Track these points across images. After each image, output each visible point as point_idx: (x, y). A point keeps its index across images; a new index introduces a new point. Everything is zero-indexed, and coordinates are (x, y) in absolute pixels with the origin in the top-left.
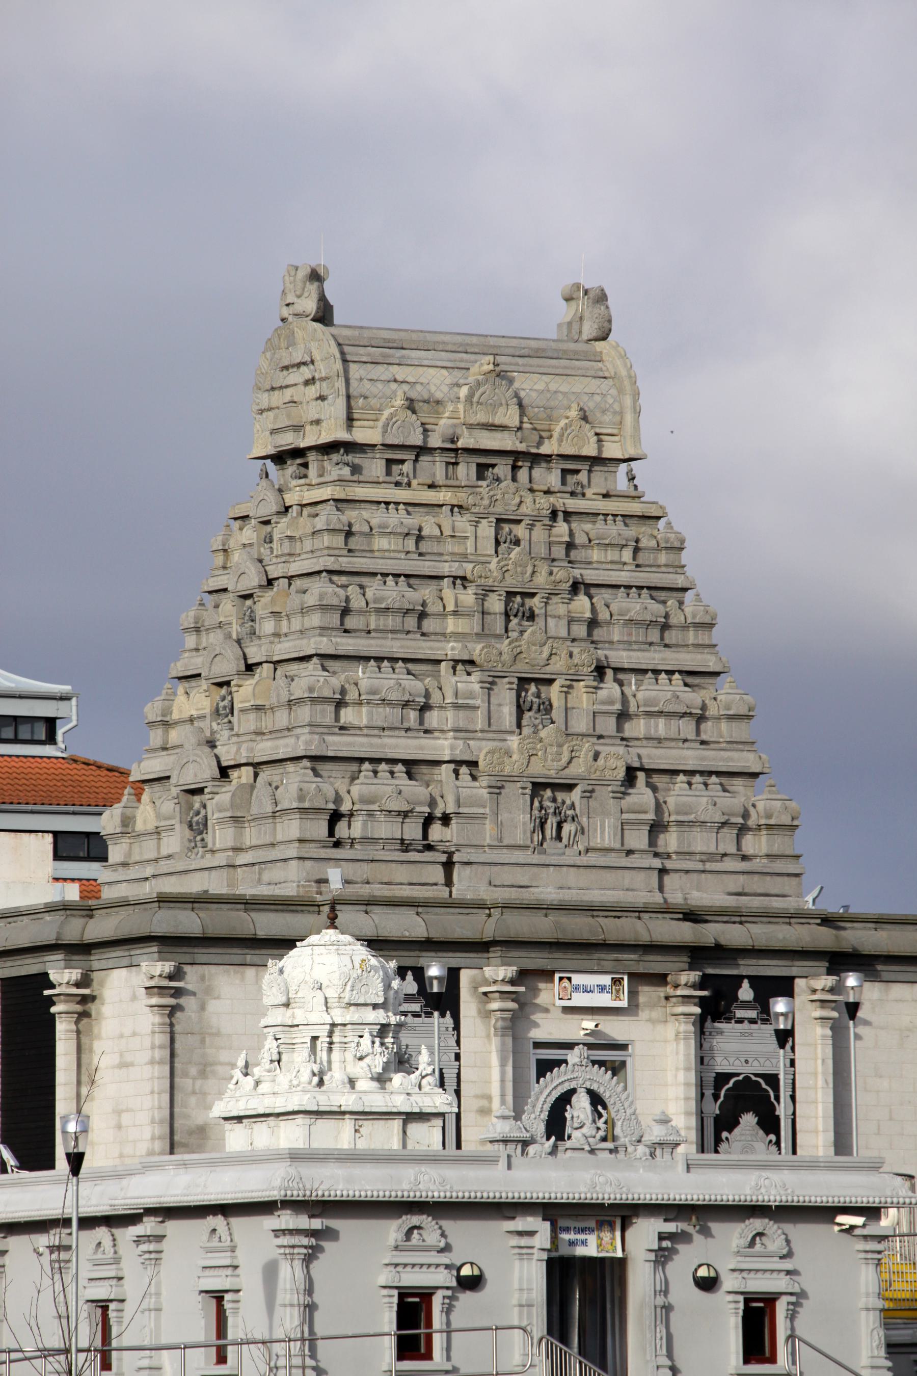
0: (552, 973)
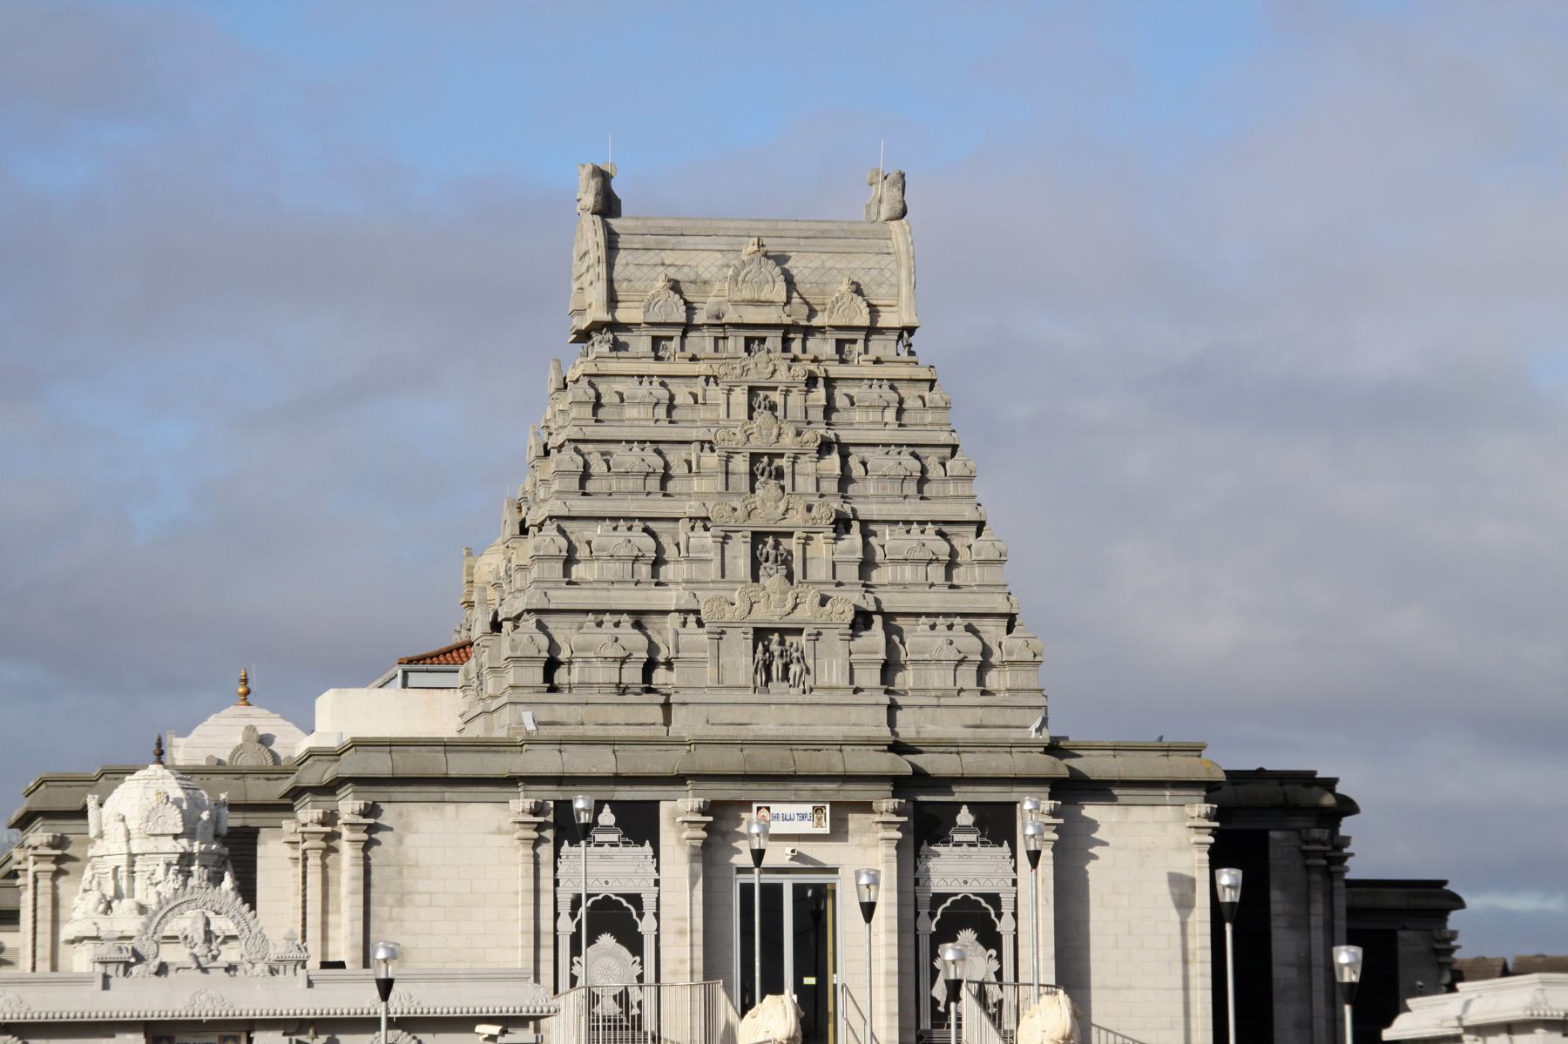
0: (751, 803)
